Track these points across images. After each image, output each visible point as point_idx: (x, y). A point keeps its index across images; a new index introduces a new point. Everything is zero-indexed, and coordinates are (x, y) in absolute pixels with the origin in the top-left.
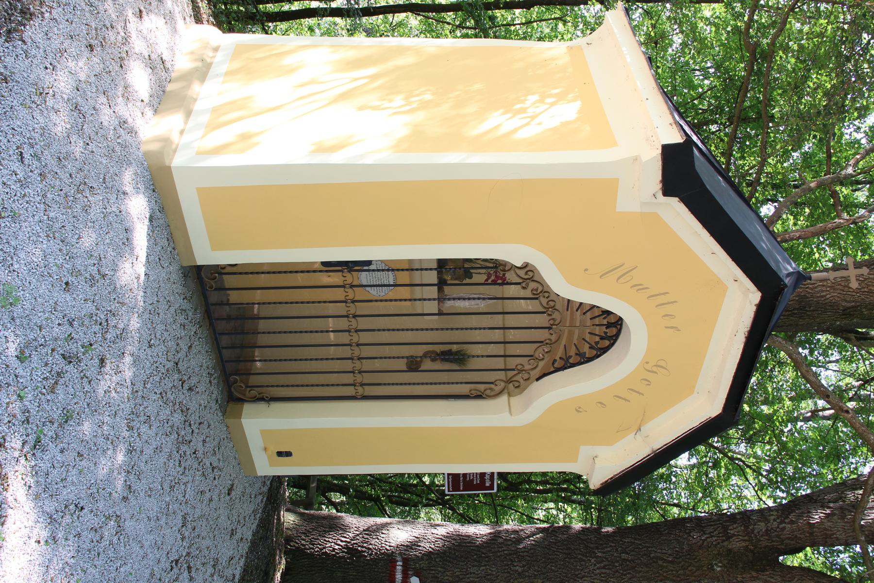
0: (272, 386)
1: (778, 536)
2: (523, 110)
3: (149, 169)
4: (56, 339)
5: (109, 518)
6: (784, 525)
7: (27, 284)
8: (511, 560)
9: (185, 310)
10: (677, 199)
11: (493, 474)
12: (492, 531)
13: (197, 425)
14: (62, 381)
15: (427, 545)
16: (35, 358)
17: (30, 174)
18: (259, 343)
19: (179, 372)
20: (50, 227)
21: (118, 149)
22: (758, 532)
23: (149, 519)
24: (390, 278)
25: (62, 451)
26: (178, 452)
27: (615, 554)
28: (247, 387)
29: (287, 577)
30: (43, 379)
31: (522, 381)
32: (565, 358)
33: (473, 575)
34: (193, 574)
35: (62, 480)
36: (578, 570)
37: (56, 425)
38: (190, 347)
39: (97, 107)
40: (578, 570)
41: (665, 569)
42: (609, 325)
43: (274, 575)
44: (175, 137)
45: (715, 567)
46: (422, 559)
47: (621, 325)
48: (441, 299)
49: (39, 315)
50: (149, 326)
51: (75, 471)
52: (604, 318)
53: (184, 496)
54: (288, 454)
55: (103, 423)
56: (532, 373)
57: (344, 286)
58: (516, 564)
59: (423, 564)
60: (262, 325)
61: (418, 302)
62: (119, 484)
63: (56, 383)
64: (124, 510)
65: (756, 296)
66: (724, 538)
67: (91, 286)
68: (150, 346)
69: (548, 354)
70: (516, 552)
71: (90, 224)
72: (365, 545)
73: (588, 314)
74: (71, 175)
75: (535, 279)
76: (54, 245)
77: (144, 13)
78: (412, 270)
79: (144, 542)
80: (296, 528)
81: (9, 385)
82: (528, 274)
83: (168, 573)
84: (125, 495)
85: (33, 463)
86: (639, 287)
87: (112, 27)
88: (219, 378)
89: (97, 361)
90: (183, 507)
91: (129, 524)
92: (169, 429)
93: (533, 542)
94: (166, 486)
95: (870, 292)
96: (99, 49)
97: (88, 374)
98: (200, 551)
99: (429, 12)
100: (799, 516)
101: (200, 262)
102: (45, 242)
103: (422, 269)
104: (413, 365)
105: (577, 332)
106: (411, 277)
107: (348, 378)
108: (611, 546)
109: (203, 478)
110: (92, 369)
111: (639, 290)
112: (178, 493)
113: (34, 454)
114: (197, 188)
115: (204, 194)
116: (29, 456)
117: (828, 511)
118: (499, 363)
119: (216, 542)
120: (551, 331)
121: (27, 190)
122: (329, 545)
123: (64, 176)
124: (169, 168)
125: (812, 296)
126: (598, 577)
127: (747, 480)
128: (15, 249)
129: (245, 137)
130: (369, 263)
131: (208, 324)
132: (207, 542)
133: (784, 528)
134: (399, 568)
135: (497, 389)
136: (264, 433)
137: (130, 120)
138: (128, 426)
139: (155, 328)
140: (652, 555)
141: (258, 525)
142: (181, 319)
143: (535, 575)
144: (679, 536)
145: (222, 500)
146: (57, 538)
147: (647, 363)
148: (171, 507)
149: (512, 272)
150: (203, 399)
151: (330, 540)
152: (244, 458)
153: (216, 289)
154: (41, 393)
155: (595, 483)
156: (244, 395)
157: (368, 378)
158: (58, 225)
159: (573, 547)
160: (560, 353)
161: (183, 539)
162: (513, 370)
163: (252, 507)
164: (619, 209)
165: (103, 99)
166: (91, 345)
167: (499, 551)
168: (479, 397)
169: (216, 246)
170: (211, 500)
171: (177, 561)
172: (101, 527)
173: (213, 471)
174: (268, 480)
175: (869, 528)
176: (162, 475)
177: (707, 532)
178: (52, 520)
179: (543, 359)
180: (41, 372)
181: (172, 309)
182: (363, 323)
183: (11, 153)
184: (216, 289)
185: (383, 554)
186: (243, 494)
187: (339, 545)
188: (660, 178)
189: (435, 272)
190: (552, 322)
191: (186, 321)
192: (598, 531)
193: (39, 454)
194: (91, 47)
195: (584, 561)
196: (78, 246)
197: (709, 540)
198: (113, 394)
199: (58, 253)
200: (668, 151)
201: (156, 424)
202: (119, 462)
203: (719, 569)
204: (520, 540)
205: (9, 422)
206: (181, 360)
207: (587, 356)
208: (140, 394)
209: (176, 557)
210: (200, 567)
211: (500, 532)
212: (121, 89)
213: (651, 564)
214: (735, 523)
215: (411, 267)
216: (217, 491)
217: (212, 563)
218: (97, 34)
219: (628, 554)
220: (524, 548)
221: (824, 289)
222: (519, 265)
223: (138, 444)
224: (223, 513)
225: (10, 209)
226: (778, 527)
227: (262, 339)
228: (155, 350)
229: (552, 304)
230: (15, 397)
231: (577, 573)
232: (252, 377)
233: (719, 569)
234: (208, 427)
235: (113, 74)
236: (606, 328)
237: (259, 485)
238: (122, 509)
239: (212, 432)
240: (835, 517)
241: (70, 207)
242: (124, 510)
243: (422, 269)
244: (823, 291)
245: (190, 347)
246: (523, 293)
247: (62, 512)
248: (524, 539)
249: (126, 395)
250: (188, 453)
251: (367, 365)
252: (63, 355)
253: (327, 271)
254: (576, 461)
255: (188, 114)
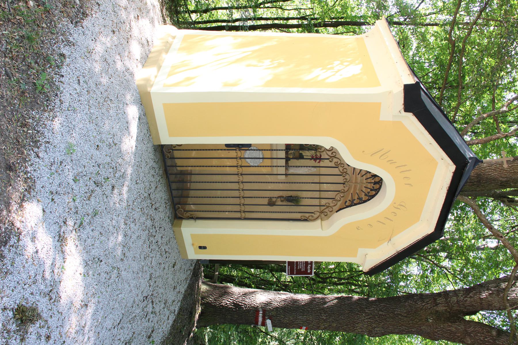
0: (197, 211)
1: (463, 305)
2: (332, 68)
3: (139, 93)
4: (91, 173)
5: (114, 268)
6: (466, 299)
7: (79, 144)
8: (320, 313)
9: (154, 168)
10: (411, 114)
11: (312, 262)
12: (310, 297)
13: (158, 228)
14: (93, 195)
15: (276, 304)
16: (81, 182)
17: (83, 90)
18: (193, 180)
19: (151, 199)
20: (91, 117)
21: (124, 82)
22: (453, 302)
23: (133, 272)
24: (259, 154)
25: (92, 231)
26: (148, 240)
27: (376, 312)
28: (184, 211)
29: (202, 317)
30: (85, 192)
31: (329, 213)
32: (351, 200)
33: (299, 320)
34: (154, 305)
35: (92, 245)
36: (356, 319)
37: (90, 217)
38: (156, 187)
39: (116, 60)
40: (356, 319)
41: (402, 320)
42: (375, 183)
43: (195, 315)
44: (152, 79)
45: (429, 320)
46: (273, 310)
47: (382, 183)
48: (287, 166)
49: (84, 160)
50: (136, 173)
51: (98, 242)
52: (373, 179)
53: (151, 264)
54: (205, 248)
55: (113, 219)
56: (334, 208)
57: (236, 158)
58: (323, 315)
59: (273, 313)
60: (194, 178)
61: (275, 168)
62: (119, 252)
63: (91, 195)
64: (121, 266)
65: (453, 167)
66: (434, 305)
67: (109, 149)
68: (137, 183)
69: (343, 198)
70: (323, 309)
71: (110, 118)
72: (243, 302)
73: (364, 176)
74: (101, 93)
75: (336, 157)
76: (92, 126)
77: (140, 17)
78: (272, 150)
79: (130, 283)
80: (207, 292)
81: (69, 193)
82: (333, 153)
83: (142, 303)
84: (122, 258)
85: (79, 234)
86: (391, 162)
87: (124, 23)
88: (170, 205)
89: (110, 187)
90: (150, 270)
91: (123, 273)
92: (145, 228)
93: (332, 304)
94: (142, 257)
95: (515, 172)
96: (117, 33)
97: (106, 193)
98: (158, 294)
99: (284, 28)
100: (475, 294)
101: (163, 143)
102: (88, 124)
103: (277, 150)
104: (271, 203)
105: (358, 186)
106: (271, 154)
107: (237, 208)
108: (374, 307)
109: (161, 256)
110: (108, 191)
111: (391, 163)
112: (148, 261)
113: (79, 230)
114: (163, 104)
115: (166, 106)
116: (77, 230)
117: (490, 292)
118: (316, 202)
119: (166, 292)
120: (344, 185)
121: (81, 98)
122: (224, 301)
123: (98, 93)
124: (149, 93)
125: (484, 175)
126: (366, 323)
127: (449, 280)
128: (74, 126)
129: (188, 79)
130: (249, 145)
131: (166, 177)
132: (161, 291)
133: (467, 300)
134: (261, 315)
135: (315, 216)
136: (193, 236)
137: (131, 68)
138: (124, 223)
139: (139, 174)
140: (395, 313)
141: (188, 287)
142: (152, 172)
143: (333, 321)
144: (410, 303)
145: (170, 269)
146: (89, 274)
147: (395, 203)
148: (144, 268)
149: (324, 153)
150: (162, 215)
151: (225, 299)
152: (181, 249)
153: (170, 158)
154: (83, 199)
155: (366, 268)
156: (183, 215)
157: (247, 208)
158: (94, 117)
159: (353, 307)
160: (350, 198)
161: (150, 286)
162: (324, 206)
163: (185, 276)
164: (381, 119)
165: (118, 57)
166: (108, 178)
167: (314, 308)
168: (306, 220)
169: (171, 135)
170: (164, 269)
171: (146, 297)
172: (110, 272)
173: (166, 253)
174: (194, 263)
175: (512, 301)
176: (140, 251)
177: (425, 301)
178: (87, 264)
179: (340, 200)
180: (84, 189)
181: (148, 166)
182: (246, 178)
183: (74, 79)
184: (170, 158)
185: (252, 307)
186: (181, 268)
187: (229, 301)
188: (403, 102)
189: (284, 152)
190: (345, 180)
191: (155, 174)
192: (367, 299)
193: (82, 230)
194: (114, 32)
195: (359, 314)
196: (103, 128)
197: (426, 305)
198: (118, 205)
199: (94, 130)
200: (408, 89)
201: (138, 224)
202: (120, 240)
203: (431, 321)
204: (325, 303)
205: (69, 212)
206: (152, 193)
207: (363, 200)
208: (131, 207)
209: (146, 295)
210: (158, 302)
211: (314, 298)
212: (127, 53)
213: (395, 317)
214: (441, 297)
215: (272, 148)
216: (167, 265)
217: (164, 302)
218: (117, 26)
219: (382, 311)
220: (327, 307)
221: (490, 170)
222: (328, 148)
223: (129, 233)
224: (171, 276)
225: (72, 106)
226: (463, 300)
227: (193, 186)
228: (139, 186)
229: (345, 170)
230: (71, 200)
231: (355, 321)
232: (189, 199)
233: (431, 321)
234: (164, 230)
235: (123, 45)
236: (374, 185)
237: (188, 265)
238: (120, 265)
239: (166, 233)
240: (494, 295)
241: (100, 109)
242: (121, 266)
243: (277, 150)
244: (490, 172)
245: (156, 187)
246: (330, 164)
247: (92, 261)
248: (328, 302)
249: (124, 206)
250: (154, 242)
251: (247, 201)
252: (94, 182)
253: (228, 150)
254: (356, 256)
255: (159, 68)
